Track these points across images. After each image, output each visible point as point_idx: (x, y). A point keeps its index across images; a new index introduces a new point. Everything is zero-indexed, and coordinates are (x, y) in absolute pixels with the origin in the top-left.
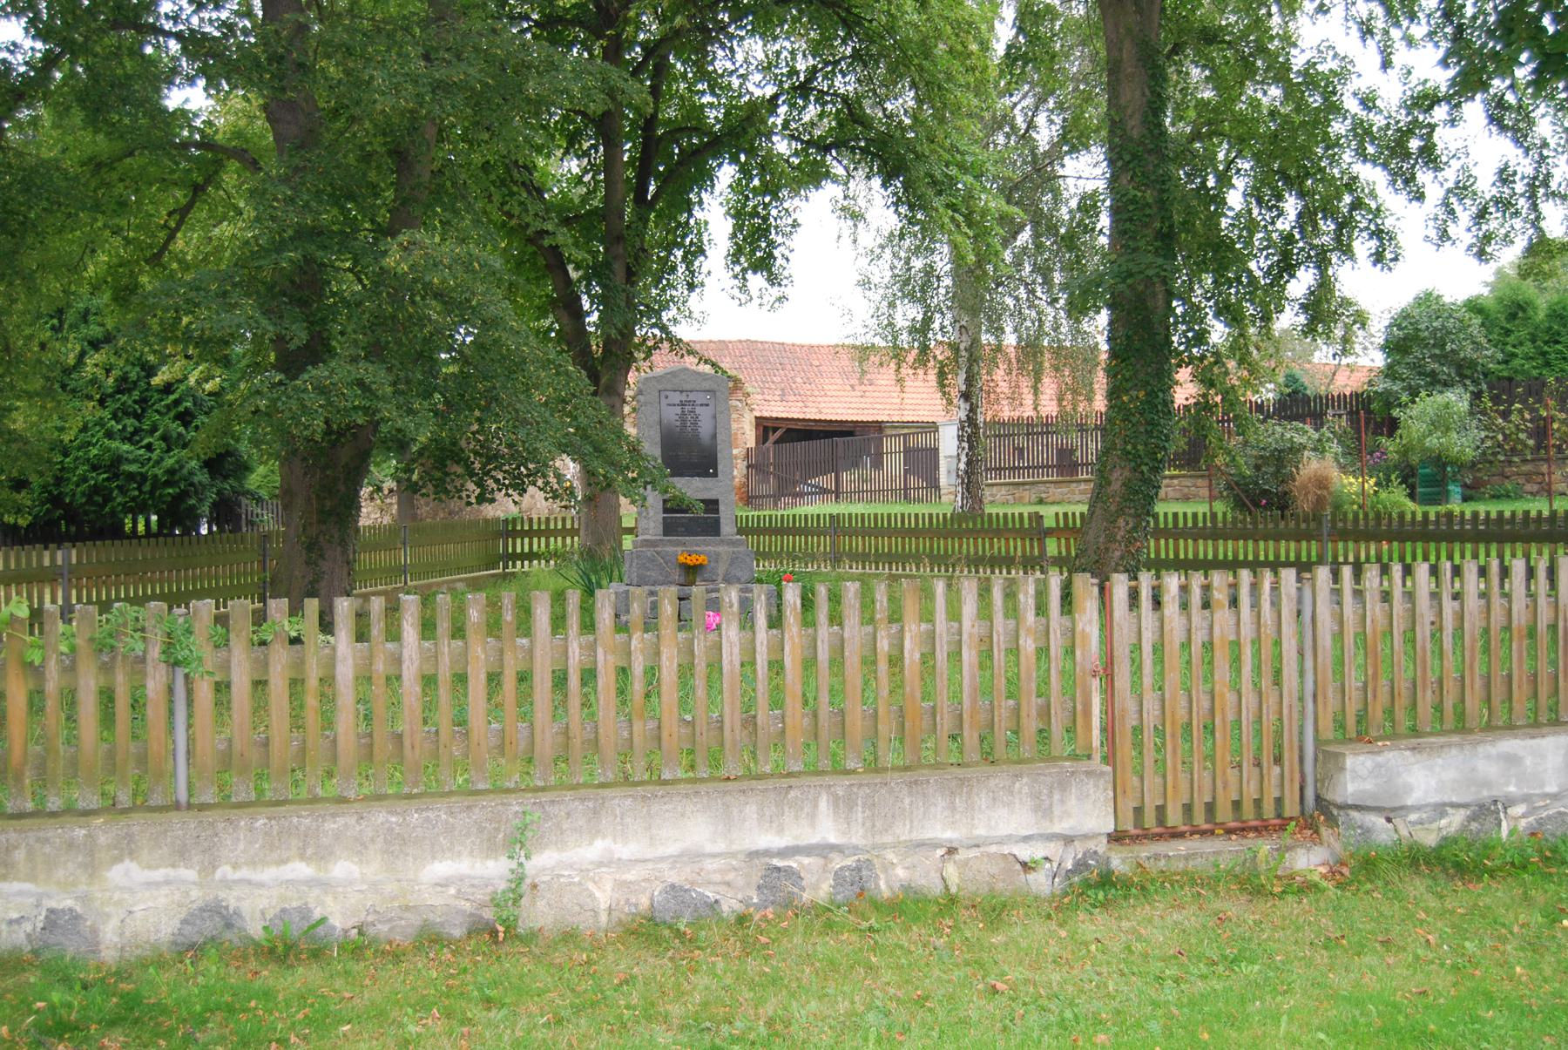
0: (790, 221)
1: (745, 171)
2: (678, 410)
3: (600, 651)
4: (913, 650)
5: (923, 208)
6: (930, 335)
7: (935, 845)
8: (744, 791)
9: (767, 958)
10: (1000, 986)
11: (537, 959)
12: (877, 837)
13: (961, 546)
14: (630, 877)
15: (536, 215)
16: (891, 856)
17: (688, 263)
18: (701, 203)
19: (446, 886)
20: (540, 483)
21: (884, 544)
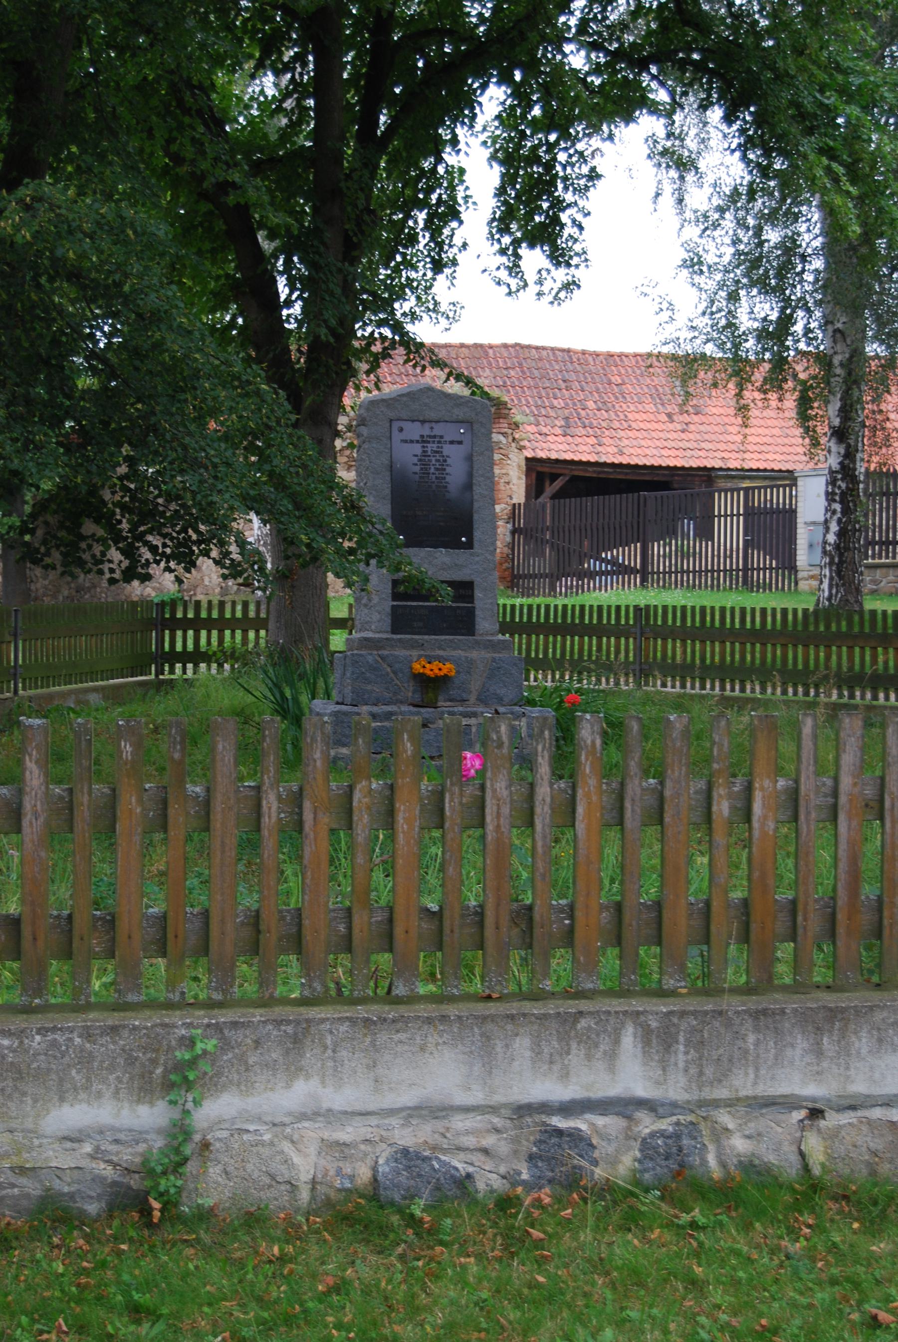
0: (585, 170)
1: (520, 94)
2: (417, 449)
3: (307, 805)
4: (765, 817)
5: (785, 154)
6: (789, 343)
7: (788, 1103)
8: (512, 1017)
9: (542, 1261)
10: (883, 1316)
11: (207, 1252)
12: (707, 1089)
13: (828, 658)
14: (345, 1134)
15: (216, 159)
16: (725, 1118)
17: (435, 233)
18: (455, 142)
19: (80, 1141)
20: (214, 554)
21: (714, 652)
